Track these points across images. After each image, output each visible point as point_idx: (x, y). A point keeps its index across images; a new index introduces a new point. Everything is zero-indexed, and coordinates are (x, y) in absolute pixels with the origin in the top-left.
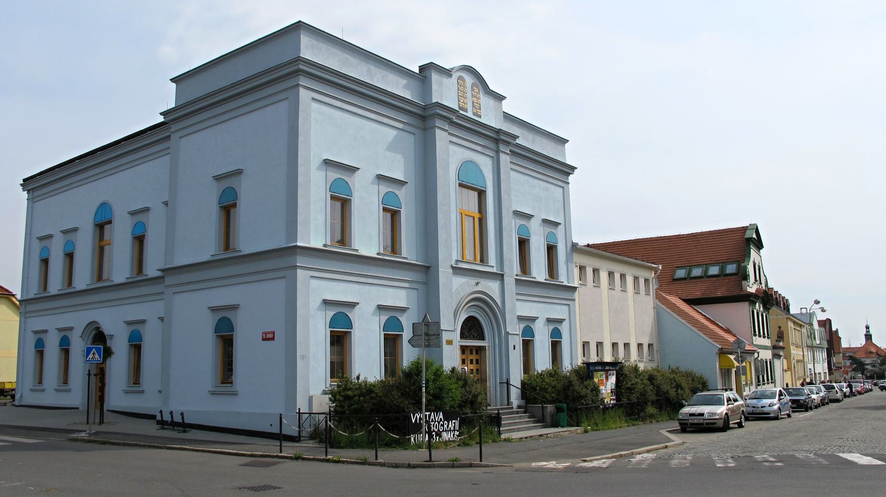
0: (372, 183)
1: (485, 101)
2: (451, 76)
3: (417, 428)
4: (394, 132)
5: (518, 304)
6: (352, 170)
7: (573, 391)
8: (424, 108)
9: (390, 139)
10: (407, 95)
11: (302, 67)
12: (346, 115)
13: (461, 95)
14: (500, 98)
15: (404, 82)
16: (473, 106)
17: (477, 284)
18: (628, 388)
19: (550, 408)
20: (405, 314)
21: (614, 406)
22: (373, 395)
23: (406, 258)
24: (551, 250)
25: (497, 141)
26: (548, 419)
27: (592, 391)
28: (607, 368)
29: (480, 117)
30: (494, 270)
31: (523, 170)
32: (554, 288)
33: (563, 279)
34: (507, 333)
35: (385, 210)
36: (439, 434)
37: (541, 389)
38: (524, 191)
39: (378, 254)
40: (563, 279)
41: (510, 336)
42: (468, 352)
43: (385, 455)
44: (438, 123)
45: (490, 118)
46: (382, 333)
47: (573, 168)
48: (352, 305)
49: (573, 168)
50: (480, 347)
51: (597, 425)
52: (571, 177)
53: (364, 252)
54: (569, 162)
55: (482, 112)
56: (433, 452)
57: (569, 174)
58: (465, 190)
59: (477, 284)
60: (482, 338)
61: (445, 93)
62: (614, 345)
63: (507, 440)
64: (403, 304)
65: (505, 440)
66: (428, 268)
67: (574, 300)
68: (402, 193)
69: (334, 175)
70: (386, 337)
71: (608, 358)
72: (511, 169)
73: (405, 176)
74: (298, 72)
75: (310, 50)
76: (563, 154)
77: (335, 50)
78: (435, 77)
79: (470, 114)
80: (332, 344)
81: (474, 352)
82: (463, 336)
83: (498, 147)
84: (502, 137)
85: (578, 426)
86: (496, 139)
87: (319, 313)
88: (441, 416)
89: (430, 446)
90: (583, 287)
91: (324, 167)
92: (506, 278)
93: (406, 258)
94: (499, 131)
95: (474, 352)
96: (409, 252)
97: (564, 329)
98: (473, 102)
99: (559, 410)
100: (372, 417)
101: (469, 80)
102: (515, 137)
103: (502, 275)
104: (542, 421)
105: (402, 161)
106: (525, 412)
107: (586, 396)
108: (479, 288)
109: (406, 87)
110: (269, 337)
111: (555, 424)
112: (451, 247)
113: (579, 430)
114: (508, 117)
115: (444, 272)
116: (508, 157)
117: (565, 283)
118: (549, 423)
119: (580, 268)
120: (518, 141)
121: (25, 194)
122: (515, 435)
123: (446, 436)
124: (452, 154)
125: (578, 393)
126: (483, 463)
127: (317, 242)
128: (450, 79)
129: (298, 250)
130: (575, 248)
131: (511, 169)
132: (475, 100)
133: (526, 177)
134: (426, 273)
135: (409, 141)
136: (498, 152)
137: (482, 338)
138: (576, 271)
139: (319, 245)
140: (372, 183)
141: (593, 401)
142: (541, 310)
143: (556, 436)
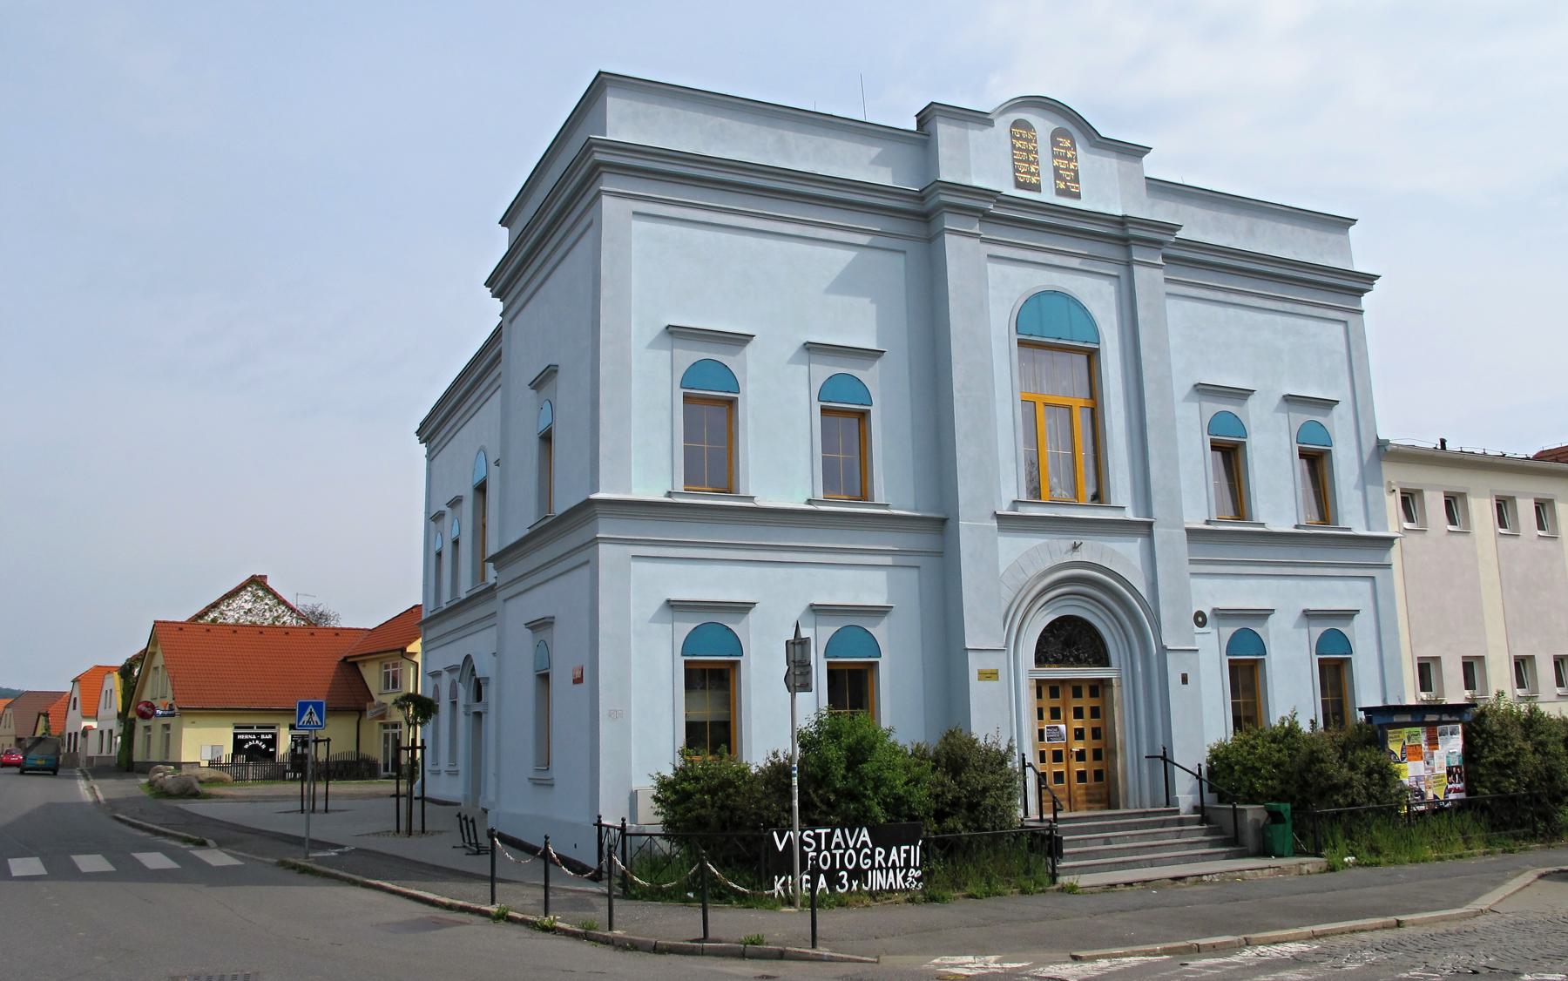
0: (792, 361)
1: (1087, 161)
2: (990, 123)
3: (783, 863)
4: (849, 255)
5: (1197, 583)
6: (1243, 394)
7: (1320, 773)
8: (920, 197)
9: (837, 269)
10: (884, 177)
11: (598, 157)
12: (724, 236)
13: (1023, 156)
14: (1138, 152)
15: (875, 151)
16: (1058, 176)
17: (1075, 547)
18: (1497, 764)
19: (1253, 813)
20: (885, 621)
21: (1461, 806)
22: (731, 790)
23: (886, 506)
24: (1316, 461)
25: (1125, 242)
26: (1250, 838)
27: (1369, 774)
28: (1430, 718)
29: (1077, 196)
30: (1129, 515)
31: (1221, 296)
32: (1323, 540)
33: (1352, 519)
34: (1163, 650)
35: (1215, 447)
36: (858, 874)
37: (1247, 770)
38: (1201, 339)
39: (809, 502)
40: (1352, 519)
41: (1169, 656)
42: (1054, 693)
43: (730, 922)
44: (950, 222)
45: (1104, 191)
46: (1226, 660)
47: (1371, 279)
48: (1263, 615)
49: (1371, 279)
50: (1101, 680)
51: (1374, 850)
52: (1366, 299)
53: (767, 499)
54: (1359, 267)
55: (1083, 187)
56: (820, 914)
57: (1362, 292)
58: (1029, 352)
59: (1075, 547)
60: (1102, 660)
61: (979, 162)
62: (1522, 666)
63: (1071, 890)
64: (880, 601)
65: (1063, 889)
66: (943, 521)
67: (1389, 566)
68: (869, 375)
69: (1213, 407)
70: (1234, 667)
71: (1455, 694)
72: (1168, 294)
73: (879, 339)
74: (597, 170)
75: (624, 123)
76: (1346, 250)
77: (1309, 231)
78: (944, 131)
79: (1047, 196)
80: (689, 686)
81: (1085, 692)
82: (1041, 658)
83: (1130, 255)
84: (1132, 232)
85: (1317, 855)
86: (1121, 239)
87: (656, 627)
88: (865, 836)
89: (814, 903)
90: (1416, 537)
91: (805, 355)
92: (1157, 530)
93: (886, 506)
94: (1123, 221)
95: (1085, 692)
96: (893, 487)
97: (1361, 635)
98: (1056, 169)
99: (1275, 817)
100: (723, 830)
101: (1043, 126)
102: (1173, 228)
103: (1150, 525)
104: (1233, 842)
105: (871, 309)
106: (1201, 822)
107: (1348, 784)
108: (1077, 557)
109: (878, 161)
110: (578, 681)
111: (1265, 851)
112: (993, 469)
113: (1310, 863)
114: (1160, 188)
115: (973, 529)
116: (1159, 274)
117: (1360, 530)
118: (1251, 847)
119: (1405, 501)
120: (1179, 234)
121: (423, 449)
122: (1084, 880)
123: (877, 880)
124: (991, 286)
125: (1330, 778)
126: (823, 950)
127: (1283, 523)
128: (989, 131)
129: (598, 508)
130: (1384, 452)
131: (1168, 294)
132: (1062, 164)
133: (1231, 311)
134: (936, 530)
135: (893, 268)
136: (1129, 264)
137: (1102, 660)
138: (1393, 503)
139: (799, 504)
140: (792, 361)
141: (1370, 797)
142: (1285, 600)
143: (1227, 878)
